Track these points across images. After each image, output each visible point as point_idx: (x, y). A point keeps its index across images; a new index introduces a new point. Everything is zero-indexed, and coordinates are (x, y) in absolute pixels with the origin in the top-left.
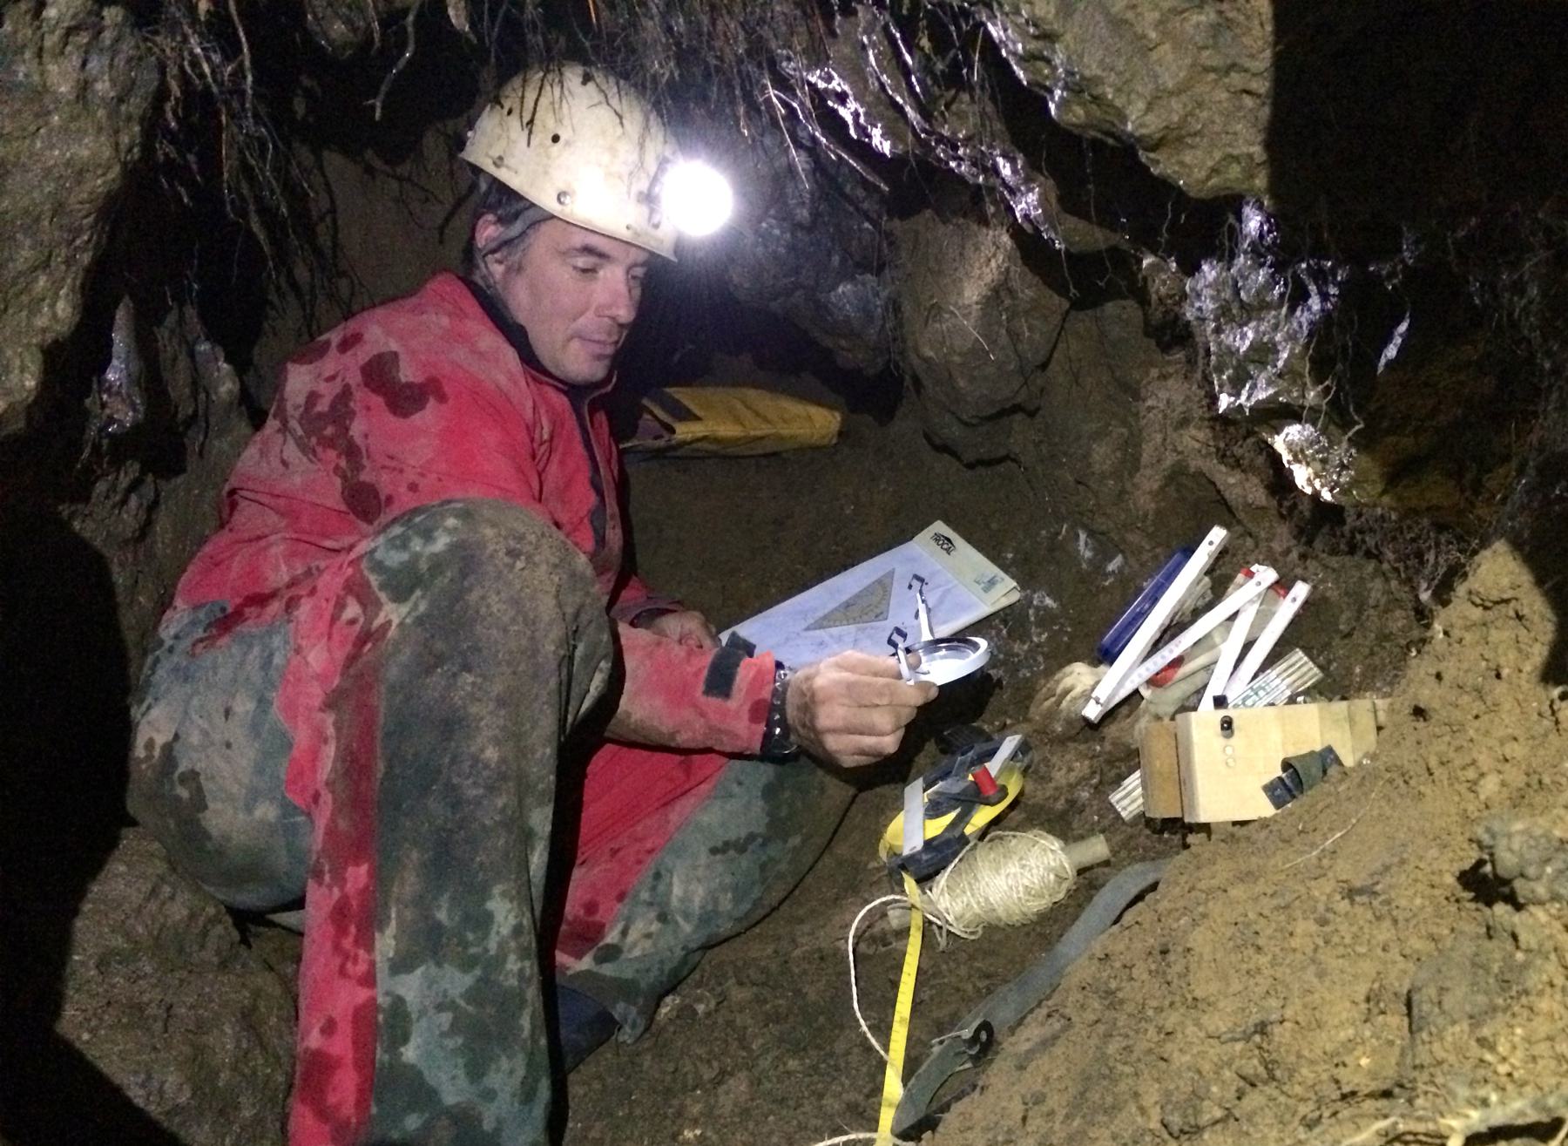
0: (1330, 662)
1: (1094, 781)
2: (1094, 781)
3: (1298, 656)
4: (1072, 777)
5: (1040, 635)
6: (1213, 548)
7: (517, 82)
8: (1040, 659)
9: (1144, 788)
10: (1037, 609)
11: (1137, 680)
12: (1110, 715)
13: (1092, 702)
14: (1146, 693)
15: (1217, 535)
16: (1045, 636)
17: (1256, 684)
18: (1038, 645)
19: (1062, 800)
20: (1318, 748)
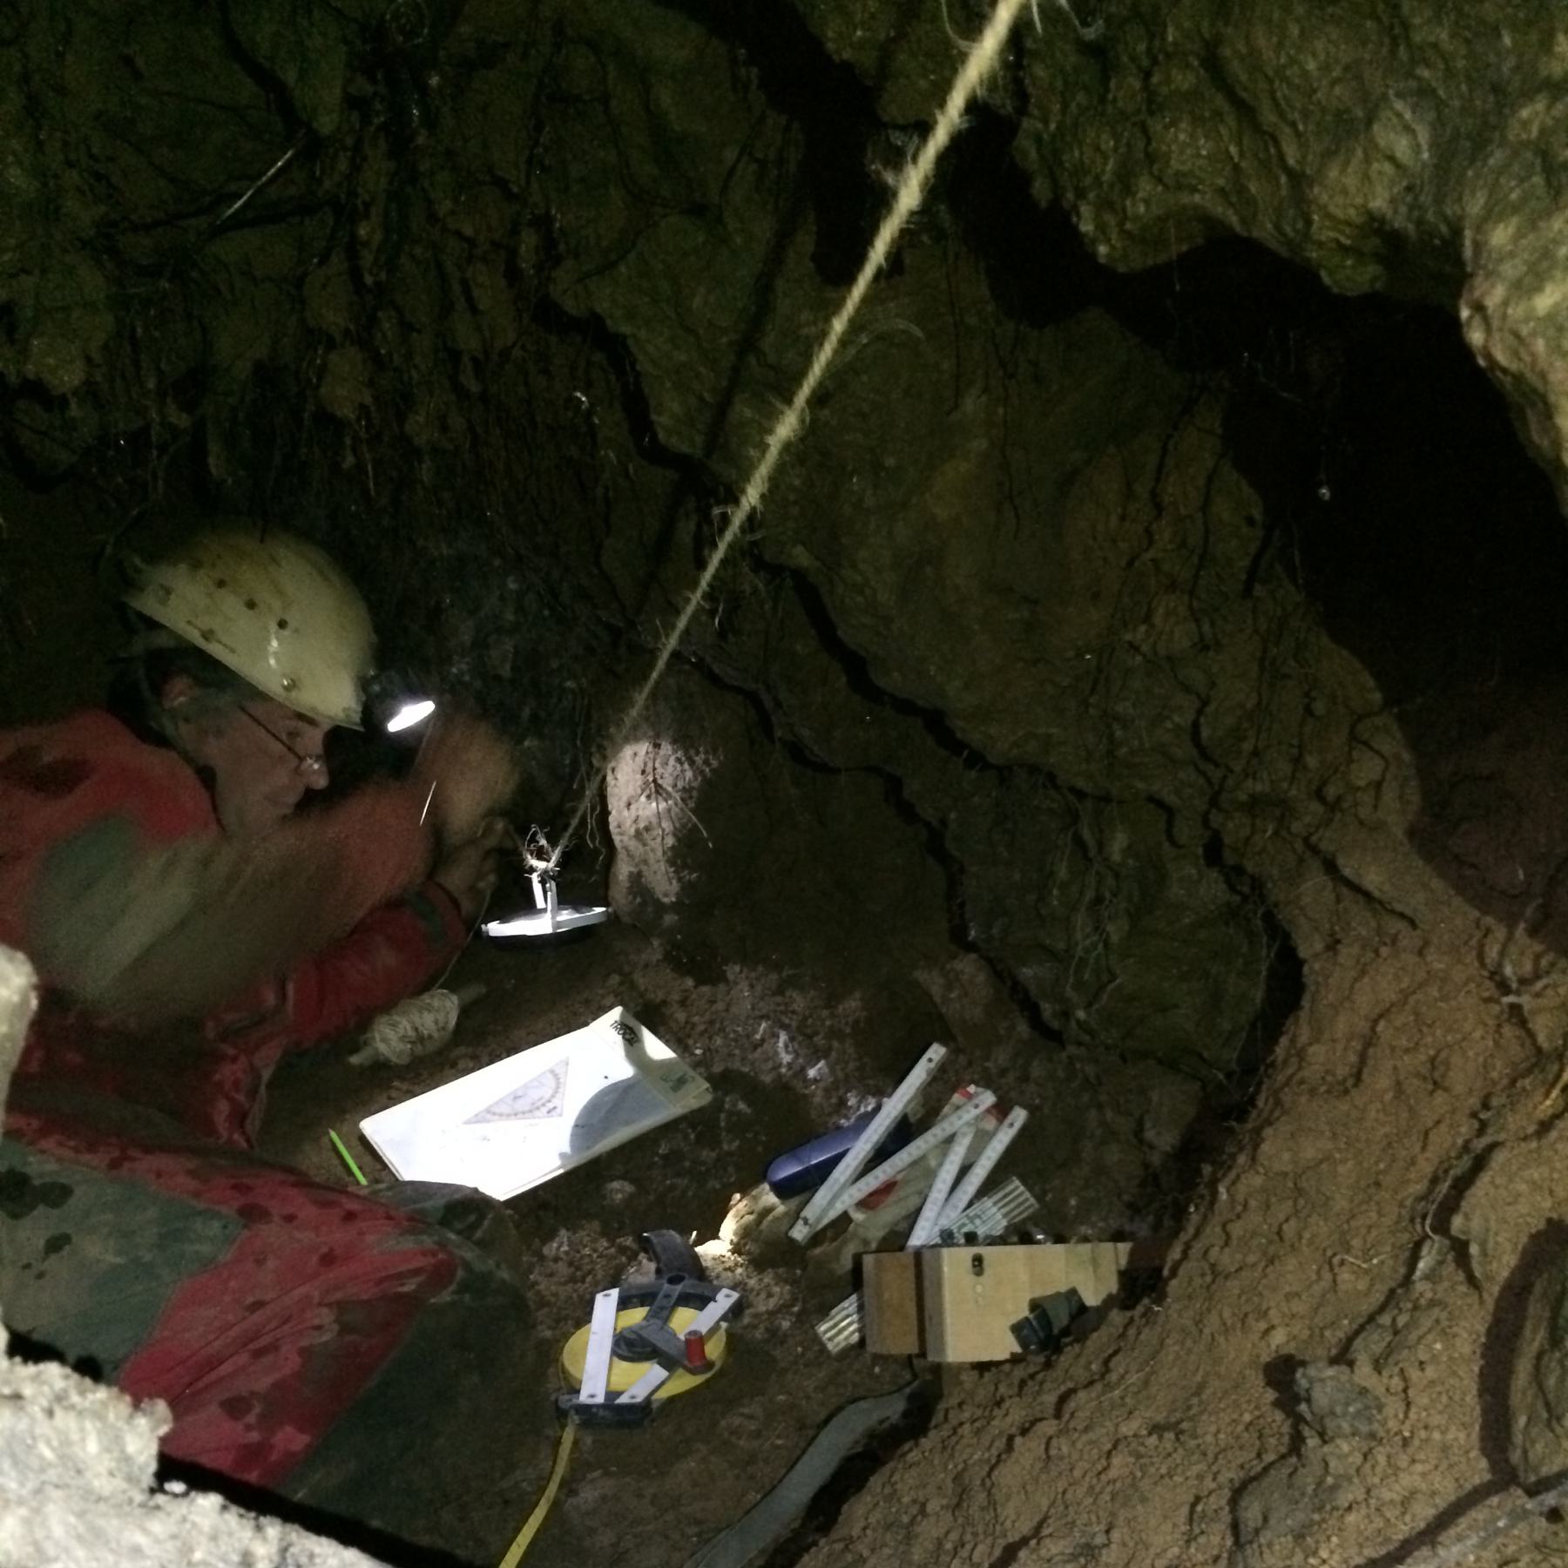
0: (1045, 1193)
1: (796, 1309)
2: (796, 1309)
3: (1015, 1185)
4: (772, 1303)
5: (730, 1142)
6: (932, 1065)
7: (1291, 1020)
8: (731, 1169)
9: (860, 1320)
10: (730, 1113)
11: (846, 1202)
12: (816, 1239)
13: (800, 1222)
14: (858, 1216)
15: (936, 1052)
16: (737, 1143)
17: (971, 1212)
18: (730, 1154)
19: (762, 1329)
20: (1063, 1289)
